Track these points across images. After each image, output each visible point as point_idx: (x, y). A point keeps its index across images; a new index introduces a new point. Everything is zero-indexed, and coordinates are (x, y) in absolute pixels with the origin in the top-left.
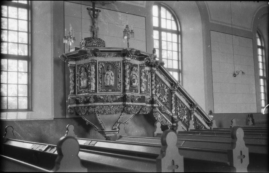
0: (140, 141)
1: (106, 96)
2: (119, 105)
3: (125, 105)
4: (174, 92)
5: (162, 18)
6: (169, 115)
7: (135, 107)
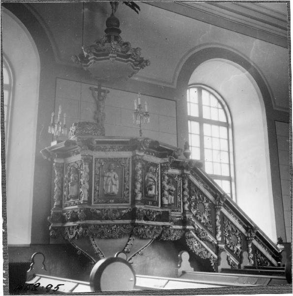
1: (105, 209)
2: (126, 224)
3: (134, 225)
4: (219, 208)
5: (204, 105)
6: (211, 242)
7: (153, 228)
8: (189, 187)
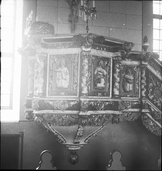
8: (147, 76)
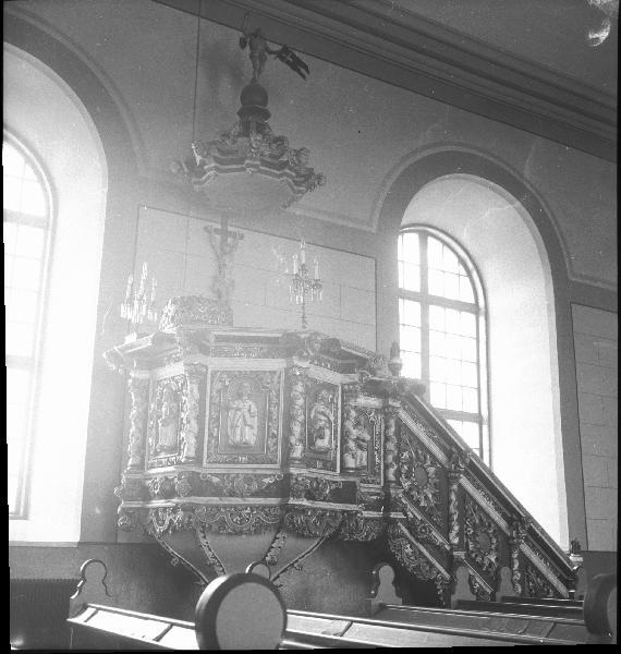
0: (306, 625)
2: (270, 507)
